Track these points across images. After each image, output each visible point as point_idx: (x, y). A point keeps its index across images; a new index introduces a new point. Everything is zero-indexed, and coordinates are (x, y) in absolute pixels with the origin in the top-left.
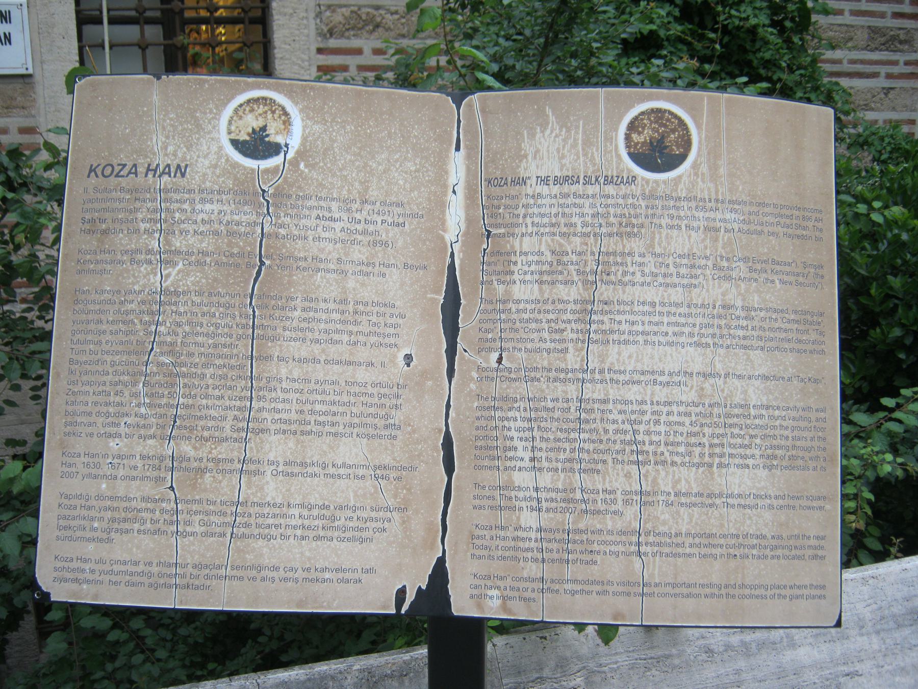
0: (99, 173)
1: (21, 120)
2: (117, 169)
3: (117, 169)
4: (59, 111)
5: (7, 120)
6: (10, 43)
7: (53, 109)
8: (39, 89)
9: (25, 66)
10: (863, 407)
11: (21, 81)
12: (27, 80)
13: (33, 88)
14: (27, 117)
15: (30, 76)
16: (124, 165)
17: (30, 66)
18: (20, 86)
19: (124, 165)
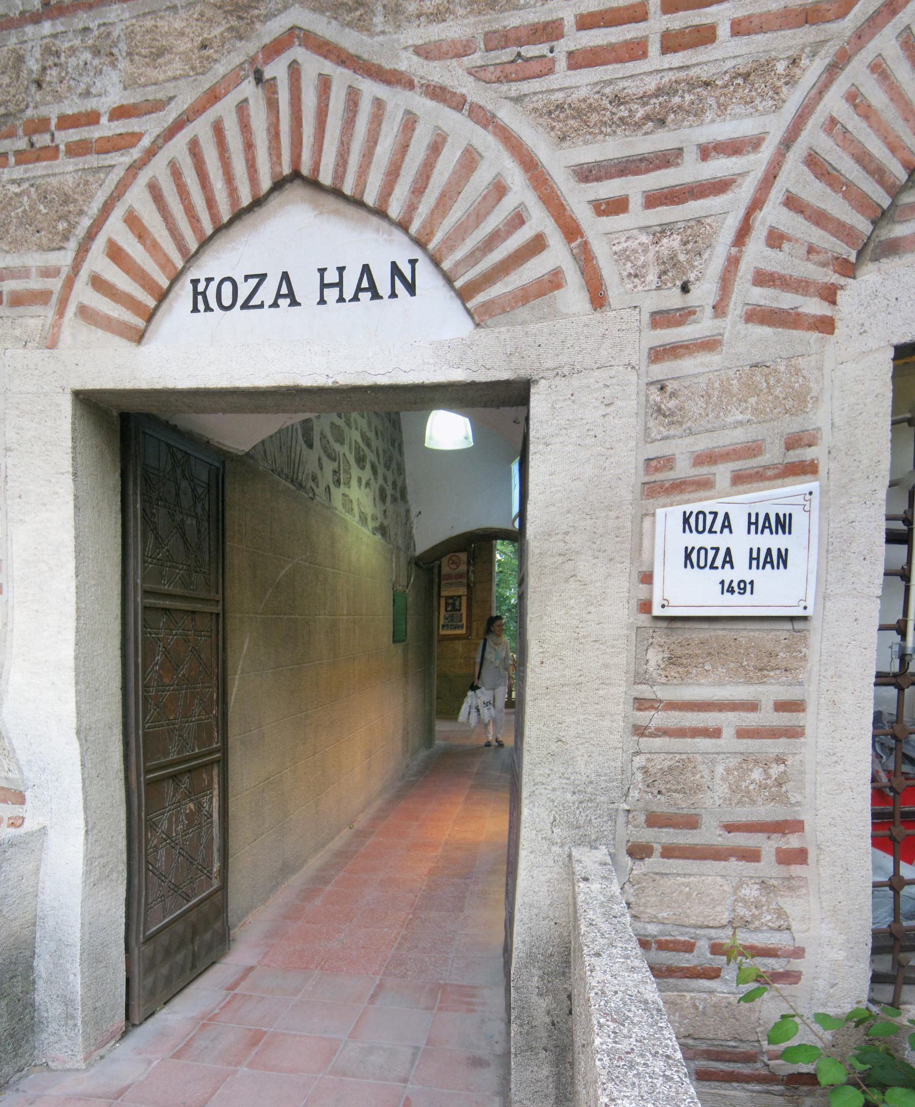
0: (213, 303)
1: (782, 689)
2: (245, 290)
3: (245, 290)
4: (840, 677)
5: (760, 688)
6: (785, 567)
7: (831, 672)
8: (814, 639)
9: (803, 604)
10: (725, 947)
11: (788, 626)
12: (799, 625)
13: (805, 638)
14: (791, 685)
15: (805, 618)
16: (262, 277)
17: (810, 604)
18: (786, 635)
19: (262, 277)
